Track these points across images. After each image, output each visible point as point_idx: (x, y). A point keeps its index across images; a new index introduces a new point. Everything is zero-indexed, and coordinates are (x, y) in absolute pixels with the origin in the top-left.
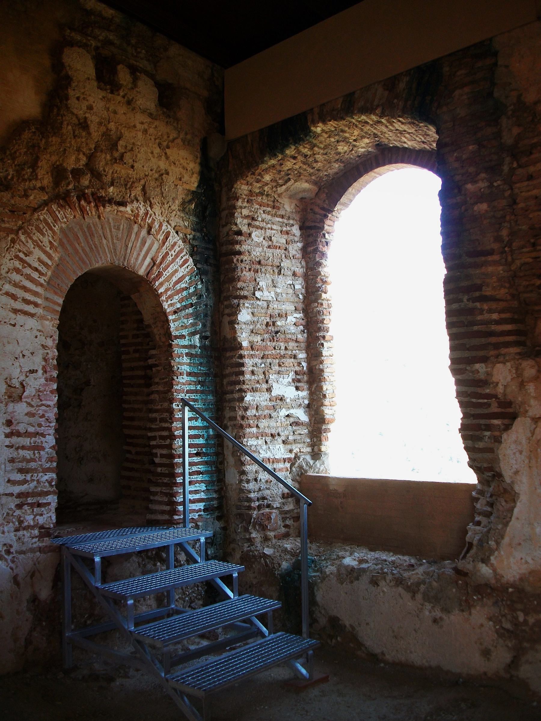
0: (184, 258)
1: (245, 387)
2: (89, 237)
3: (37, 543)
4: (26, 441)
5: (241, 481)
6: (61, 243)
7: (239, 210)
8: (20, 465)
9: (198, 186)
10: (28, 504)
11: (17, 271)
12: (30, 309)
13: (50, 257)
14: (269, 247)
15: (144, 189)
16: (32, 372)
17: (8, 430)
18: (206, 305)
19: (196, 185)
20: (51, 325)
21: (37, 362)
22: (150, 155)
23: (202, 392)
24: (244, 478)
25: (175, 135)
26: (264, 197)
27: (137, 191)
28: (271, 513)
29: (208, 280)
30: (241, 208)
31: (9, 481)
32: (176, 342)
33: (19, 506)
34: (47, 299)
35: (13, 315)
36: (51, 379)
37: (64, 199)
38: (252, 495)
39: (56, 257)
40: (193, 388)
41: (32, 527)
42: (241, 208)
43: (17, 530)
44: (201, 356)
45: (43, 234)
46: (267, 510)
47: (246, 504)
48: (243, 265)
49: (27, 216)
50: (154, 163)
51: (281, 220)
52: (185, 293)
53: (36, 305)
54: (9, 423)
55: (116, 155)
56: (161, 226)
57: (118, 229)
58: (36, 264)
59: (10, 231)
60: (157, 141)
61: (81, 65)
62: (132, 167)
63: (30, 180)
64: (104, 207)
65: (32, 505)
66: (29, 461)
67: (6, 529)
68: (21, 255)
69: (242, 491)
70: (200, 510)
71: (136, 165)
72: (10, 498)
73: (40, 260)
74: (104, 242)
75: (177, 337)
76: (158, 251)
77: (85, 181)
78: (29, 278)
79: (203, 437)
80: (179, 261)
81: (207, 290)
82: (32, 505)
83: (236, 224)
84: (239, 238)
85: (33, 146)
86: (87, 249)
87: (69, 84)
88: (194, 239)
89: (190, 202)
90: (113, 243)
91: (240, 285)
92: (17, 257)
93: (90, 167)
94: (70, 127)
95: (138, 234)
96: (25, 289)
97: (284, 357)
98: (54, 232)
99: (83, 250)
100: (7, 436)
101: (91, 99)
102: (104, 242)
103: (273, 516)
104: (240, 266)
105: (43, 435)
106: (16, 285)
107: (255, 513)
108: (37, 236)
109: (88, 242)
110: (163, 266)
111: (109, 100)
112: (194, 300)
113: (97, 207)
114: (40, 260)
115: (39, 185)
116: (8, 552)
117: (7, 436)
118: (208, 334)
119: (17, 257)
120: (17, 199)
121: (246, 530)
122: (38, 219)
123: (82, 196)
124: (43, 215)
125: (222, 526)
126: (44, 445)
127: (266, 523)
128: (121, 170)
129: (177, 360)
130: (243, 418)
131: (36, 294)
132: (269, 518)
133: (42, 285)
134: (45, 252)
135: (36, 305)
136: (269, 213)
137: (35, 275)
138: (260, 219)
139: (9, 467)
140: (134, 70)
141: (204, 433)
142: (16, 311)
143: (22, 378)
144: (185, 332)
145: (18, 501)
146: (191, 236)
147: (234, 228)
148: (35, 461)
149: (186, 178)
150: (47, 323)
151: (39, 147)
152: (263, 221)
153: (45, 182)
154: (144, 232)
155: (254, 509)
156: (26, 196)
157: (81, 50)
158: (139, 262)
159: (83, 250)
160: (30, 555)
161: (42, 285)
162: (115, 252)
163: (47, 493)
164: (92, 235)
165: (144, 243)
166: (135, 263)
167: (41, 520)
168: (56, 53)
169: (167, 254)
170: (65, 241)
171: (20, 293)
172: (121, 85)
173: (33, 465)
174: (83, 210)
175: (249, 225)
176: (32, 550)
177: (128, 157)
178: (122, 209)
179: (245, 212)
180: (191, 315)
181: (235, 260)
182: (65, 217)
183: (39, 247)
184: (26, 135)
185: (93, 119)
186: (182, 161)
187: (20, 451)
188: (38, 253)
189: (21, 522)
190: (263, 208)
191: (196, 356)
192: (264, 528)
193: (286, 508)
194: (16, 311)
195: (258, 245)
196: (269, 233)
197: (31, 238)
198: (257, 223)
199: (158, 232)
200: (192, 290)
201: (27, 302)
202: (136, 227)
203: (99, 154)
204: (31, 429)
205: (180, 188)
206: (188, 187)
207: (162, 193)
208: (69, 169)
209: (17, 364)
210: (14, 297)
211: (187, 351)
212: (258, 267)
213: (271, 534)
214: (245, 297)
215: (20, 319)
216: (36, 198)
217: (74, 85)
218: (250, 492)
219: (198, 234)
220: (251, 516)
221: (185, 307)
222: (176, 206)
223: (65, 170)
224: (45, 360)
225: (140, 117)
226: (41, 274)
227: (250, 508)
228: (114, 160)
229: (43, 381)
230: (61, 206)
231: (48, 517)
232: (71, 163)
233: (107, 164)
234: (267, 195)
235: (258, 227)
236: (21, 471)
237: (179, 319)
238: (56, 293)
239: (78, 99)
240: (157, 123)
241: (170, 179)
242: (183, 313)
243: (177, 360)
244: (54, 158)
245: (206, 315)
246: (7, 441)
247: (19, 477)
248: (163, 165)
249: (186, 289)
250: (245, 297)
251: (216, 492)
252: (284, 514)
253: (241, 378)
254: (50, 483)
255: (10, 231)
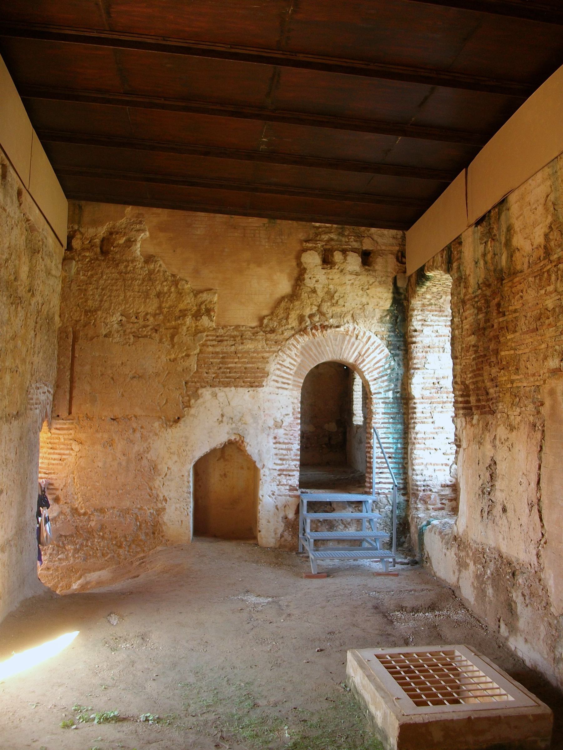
0: (381, 349)
1: (416, 421)
2: (318, 347)
3: (288, 493)
4: (284, 446)
5: (413, 474)
6: (302, 353)
7: (415, 317)
8: (280, 457)
9: (391, 306)
10: (284, 474)
11: (278, 369)
12: (286, 386)
13: (295, 361)
14: (437, 336)
15: (352, 316)
16: (287, 415)
17: (274, 441)
18: (398, 374)
19: (389, 305)
20: (298, 394)
21: (290, 410)
22: (356, 297)
23: (393, 423)
24: (414, 473)
25: (374, 281)
26: (433, 306)
27: (349, 317)
28: (431, 495)
29: (400, 360)
30: (416, 315)
31: (275, 463)
32: (374, 396)
33: (279, 475)
34: (294, 381)
35: (276, 390)
36: (297, 418)
37: (303, 331)
38: (418, 483)
39: (299, 360)
40: (386, 421)
41: (286, 485)
42: (416, 315)
43: (278, 485)
44: (393, 403)
45: (291, 350)
46: (430, 493)
47: (416, 488)
48: (418, 349)
49: (283, 343)
50: (358, 300)
51: (445, 318)
52: (381, 369)
53: (288, 384)
54: (275, 438)
55: (334, 301)
56: (365, 333)
57: (336, 340)
58: (288, 365)
59: (274, 352)
60: (361, 287)
61: (312, 260)
62: (344, 306)
63: (285, 325)
64: (326, 330)
65: (286, 475)
66: (284, 455)
67: (272, 484)
68: (281, 362)
69: (413, 480)
70: (389, 489)
71: (346, 304)
72: (275, 471)
73: (290, 363)
74: (327, 348)
75: (375, 394)
76: (363, 348)
77: (316, 319)
78: (285, 372)
79: (393, 448)
80: (378, 351)
81: (399, 365)
82: (286, 475)
83: (413, 326)
84: (415, 334)
85: (287, 309)
86: (317, 354)
87: (305, 272)
88: (389, 337)
89: (386, 316)
90: (333, 348)
91: (415, 361)
92: (278, 363)
93: (319, 311)
94: (306, 294)
95: (349, 341)
96: (283, 377)
97: (444, 403)
98: (297, 348)
99: (315, 355)
100: (274, 443)
101: (318, 277)
102: (327, 348)
103: (432, 497)
104: (415, 350)
105: (292, 444)
106: (278, 376)
107: (421, 494)
108: (288, 352)
109: (317, 350)
110: (366, 355)
111: (329, 273)
112: (389, 371)
113: (322, 331)
114: (290, 363)
115: (290, 327)
116: (273, 494)
117: (274, 443)
118: (399, 390)
119: (278, 363)
120: (278, 336)
121: (416, 503)
122: (289, 344)
123: (314, 327)
124: (292, 341)
125: (406, 499)
126: (293, 448)
127: (427, 500)
128: (337, 310)
129: (375, 406)
130: (415, 438)
131: (288, 379)
132: (430, 498)
133: (291, 375)
134: (292, 359)
135: (288, 384)
136: (436, 316)
137: (288, 370)
138: (429, 320)
139: (275, 457)
140: (344, 252)
141: (394, 446)
142: (278, 388)
143: (281, 418)
144: (381, 390)
145: (279, 473)
146: (387, 336)
147: (412, 328)
148: (287, 455)
149: (382, 303)
150: (294, 392)
151: (289, 308)
152: (431, 321)
153: (294, 325)
154: (353, 339)
155: (420, 491)
156: (283, 333)
157: (312, 252)
158: (350, 355)
159: (315, 355)
160: (283, 497)
161: (291, 375)
162: (334, 353)
163: (294, 470)
164: (320, 346)
165: (353, 344)
166: (347, 357)
167: (290, 482)
168: (298, 257)
169: (369, 348)
170: (304, 352)
171: (280, 380)
172: (337, 263)
173: (286, 457)
174: (314, 335)
175: (422, 325)
176: (285, 495)
177: (341, 302)
178: (338, 329)
179: (419, 318)
180: (386, 380)
181: (412, 347)
182: (304, 340)
183: (289, 356)
184: (283, 304)
185: (319, 287)
186: (378, 294)
187: (280, 451)
188: (289, 360)
189: (280, 482)
190: (432, 313)
191: (389, 403)
192: (426, 503)
193: (443, 493)
194: (278, 388)
195: (428, 336)
196: (436, 328)
197: (285, 353)
198: (427, 323)
199: (362, 338)
200: (387, 366)
201: (284, 383)
202: (348, 338)
203: (323, 304)
204: (286, 441)
205: (377, 310)
206: (383, 308)
207: (365, 315)
208: (307, 315)
209: (279, 411)
210: (277, 381)
211: (383, 400)
212: (429, 349)
213: (430, 507)
214: (418, 369)
215: (281, 391)
216: (287, 334)
217: (307, 272)
218: (417, 481)
219: (392, 334)
220: (418, 495)
221: (383, 376)
222: (375, 321)
223: (304, 316)
224: (294, 409)
225: (349, 277)
226: (291, 369)
227: (417, 490)
228: (333, 305)
229: (292, 419)
230: (301, 335)
231: (295, 481)
232: (307, 312)
233: (328, 308)
234: (435, 305)
235: (428, 326)
236: (281, 459)
237: (377, 383)
238: (299, 377)
239: (310, 278)
240: (360, 277)
241: (370, 308)
242: (380, 380)
243: (375, 406)
244: (298, 312)
245: (397, 380)
246: (274, 446)
247: (280, 462)
248: (364, 300)
249: (382, 366)
250: (418, 369)
251: (402, 479)
252: (442, 497)
253: (415, 416)
254: (295, 466)
255: (274, 352)
